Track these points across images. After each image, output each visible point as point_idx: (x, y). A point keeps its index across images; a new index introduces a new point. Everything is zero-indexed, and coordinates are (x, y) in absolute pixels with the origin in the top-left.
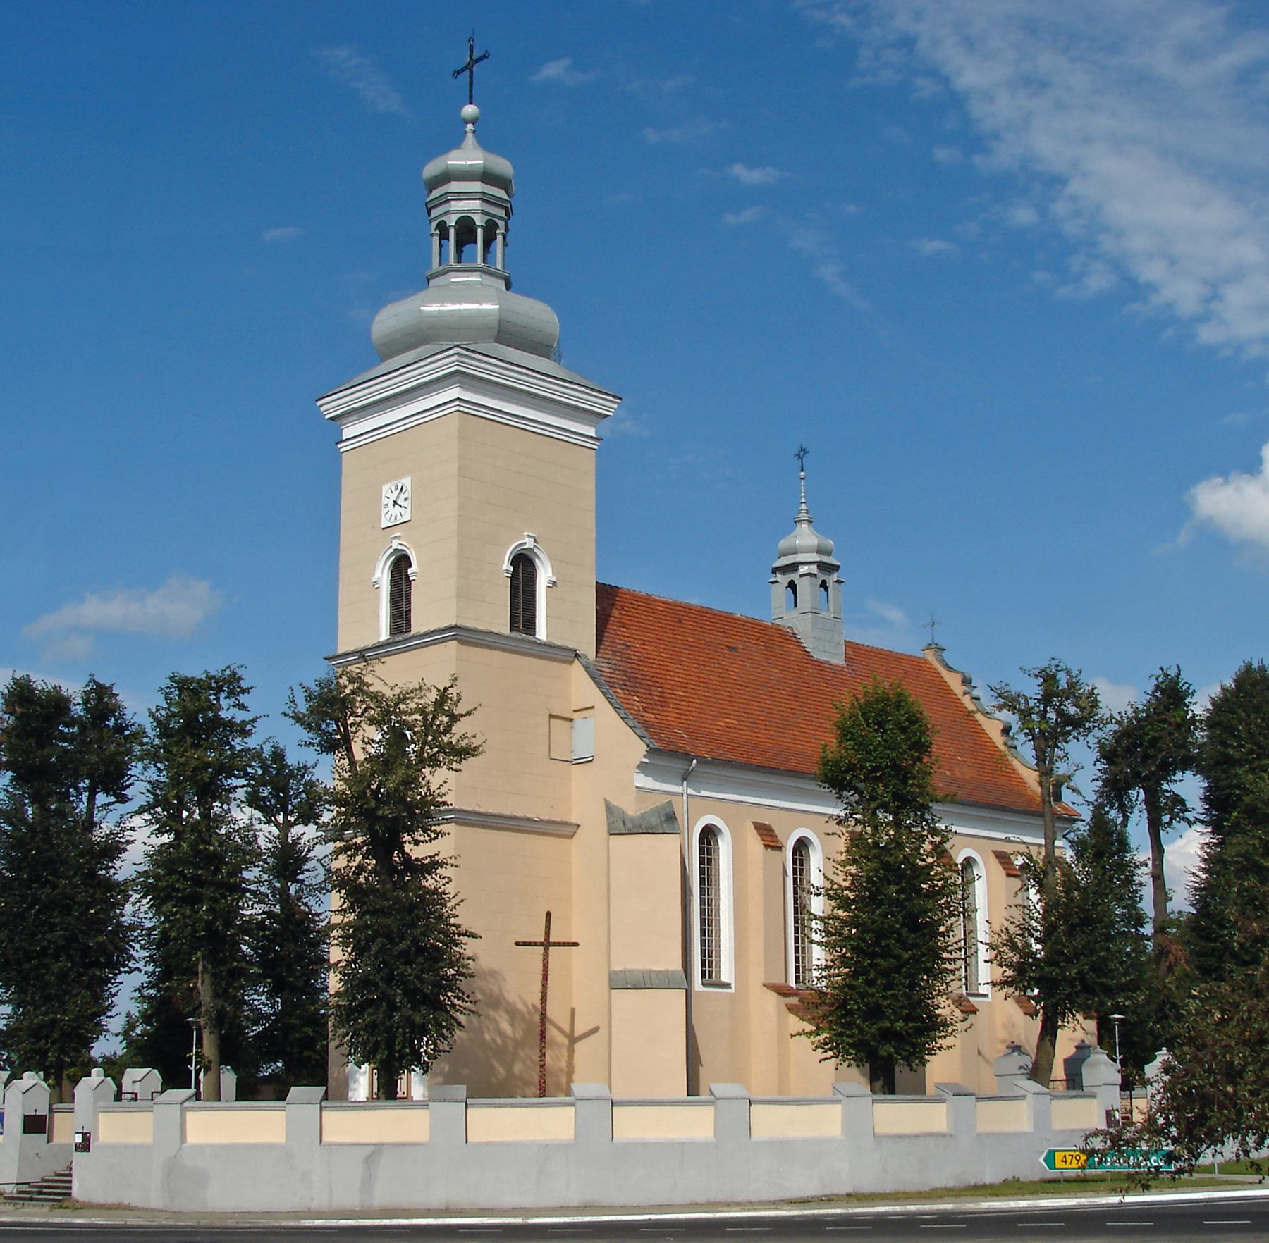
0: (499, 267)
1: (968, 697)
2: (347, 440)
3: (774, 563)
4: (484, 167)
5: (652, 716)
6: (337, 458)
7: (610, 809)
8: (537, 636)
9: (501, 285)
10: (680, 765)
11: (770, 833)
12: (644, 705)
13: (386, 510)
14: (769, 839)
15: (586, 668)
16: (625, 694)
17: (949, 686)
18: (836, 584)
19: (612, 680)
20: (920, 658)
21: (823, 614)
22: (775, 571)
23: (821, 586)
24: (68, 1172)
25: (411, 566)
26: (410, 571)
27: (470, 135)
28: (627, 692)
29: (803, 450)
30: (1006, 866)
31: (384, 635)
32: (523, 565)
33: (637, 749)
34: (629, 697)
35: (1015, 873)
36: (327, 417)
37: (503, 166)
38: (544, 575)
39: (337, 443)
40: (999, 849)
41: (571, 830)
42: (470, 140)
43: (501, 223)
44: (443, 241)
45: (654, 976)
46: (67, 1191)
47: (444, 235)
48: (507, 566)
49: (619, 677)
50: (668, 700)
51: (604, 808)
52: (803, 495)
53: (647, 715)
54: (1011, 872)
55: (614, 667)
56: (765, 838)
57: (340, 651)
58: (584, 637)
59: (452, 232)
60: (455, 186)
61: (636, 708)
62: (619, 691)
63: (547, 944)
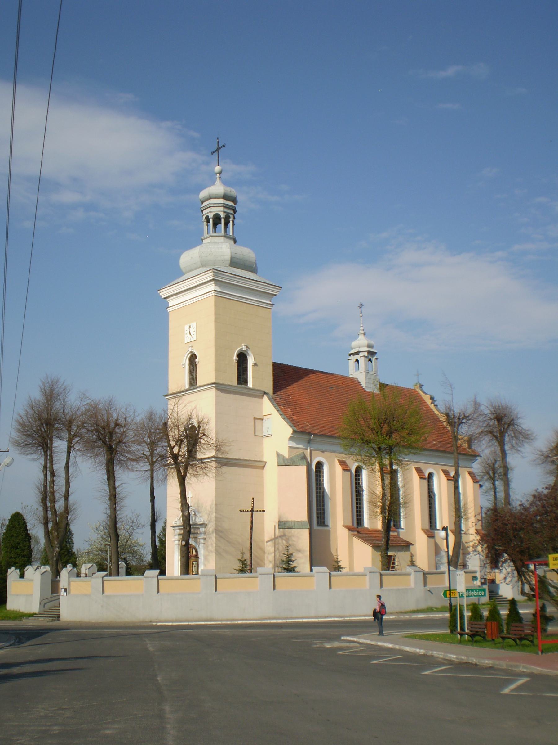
0: (231, 234)
1: (433, 405)
2: (171, 307)
3: (349, 352)
4: (224, 193)
5: (296, 417)
6: (167, 314)
7: (278, 455)
8: (248, 386)
9: (232, 242)
10: (306, 437)
11: (345, 464)
12: (293, 413)
13: (194, 330)
14: (345, 466)
15: (269, 398)
16: (285, 408)
17: (425, 401)
18: (376, 360)
19: (279, 403)
20: (413, 389)
21: (370, 373)
22: (350, 355)
23: (369, 361)
24: (58, 606)
25: (196, 358)
26: (196, 360)
27: (218, 179)
28: (285, 408)
29: (361, 304)
30: (447, 476)
31: (187, 387)
32: (242, 358)
33: (289, 431)
34: (287, 410)
35: (451, 479)
36: (163, 297)
37: (233, 192)
38: (251, 361)
39: (167, 308)
40: (444, 469)
41: (262, 464)
42: (218, 181)
43: (231, 216)
44: (208, 223)
45: (296, 523)
46: (58, 611)
47: (208, 221)
48: (235, 358)
49: (282, 401)
50: (303, 410)
51: (276, 455)
52: (361, 323)
53: (294, 417)
54: (449, 478)
55: (280, 397)
56: (343, 466)
57: (170, 393)
58: (268, 385)
59: (211, 220)
60: (212, 201)
61: (289, 414)
62: (282, 407)
63: (252, 511)
